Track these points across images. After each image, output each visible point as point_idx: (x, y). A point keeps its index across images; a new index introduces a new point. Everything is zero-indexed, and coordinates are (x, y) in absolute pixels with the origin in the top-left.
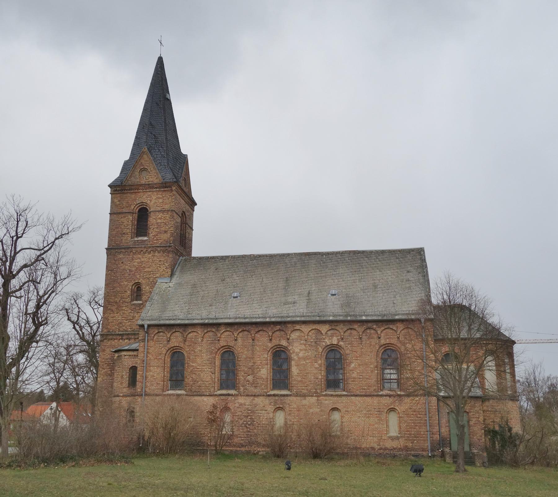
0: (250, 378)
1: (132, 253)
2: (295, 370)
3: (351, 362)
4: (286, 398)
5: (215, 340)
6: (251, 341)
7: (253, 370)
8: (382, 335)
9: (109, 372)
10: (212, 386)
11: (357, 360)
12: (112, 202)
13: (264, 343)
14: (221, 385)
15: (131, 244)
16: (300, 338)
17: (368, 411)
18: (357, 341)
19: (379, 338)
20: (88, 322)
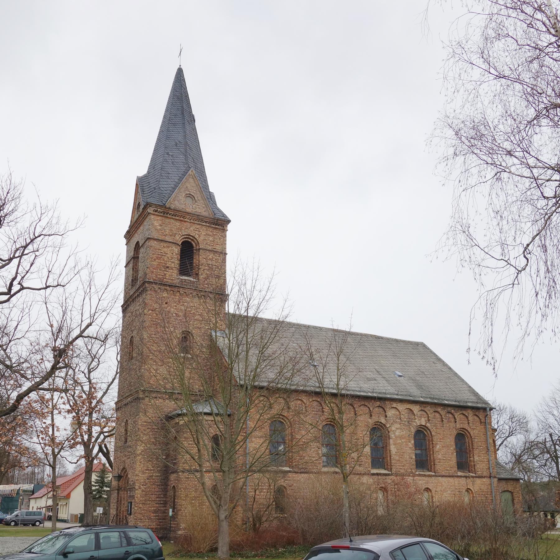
2: (393, 449)
3: (437, 444)
4: (387, 477)
15: (176, 282)
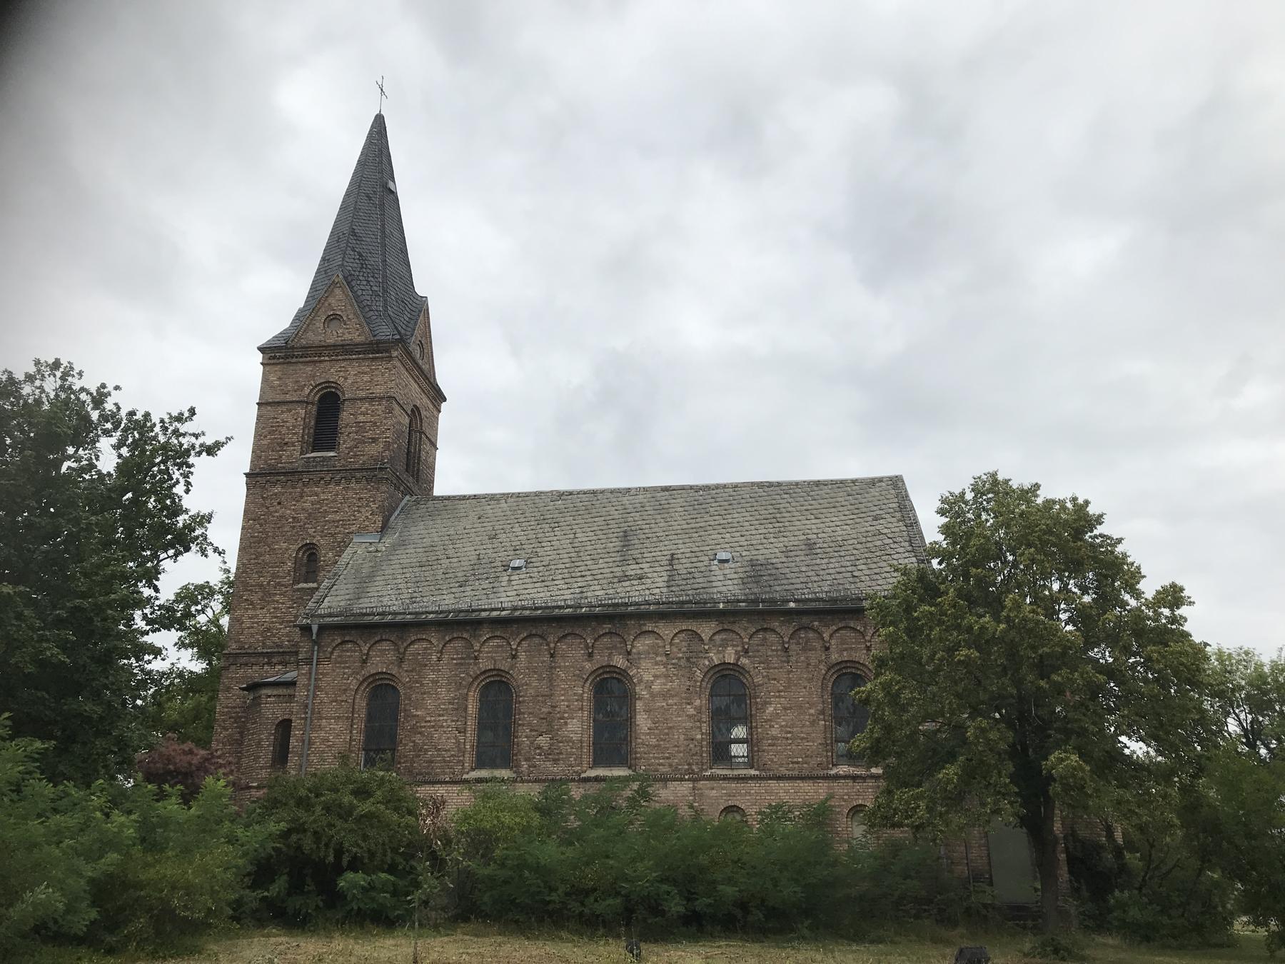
0: (543, 741)
1: (300, 484)
2: (643, 721)
3: (766, 703)
5: (469, 657)
6: (547, 658)
7: (550, 723)
8: (833, 642)
9: (237, 736)
10: (459, 761)
11: (779, 697)
12: (265, 380)
13: (572, 669)
14: (479, 755)
15: (298, 465)
16: (654, 651)
18: (778, 656)
19: (827, 649)
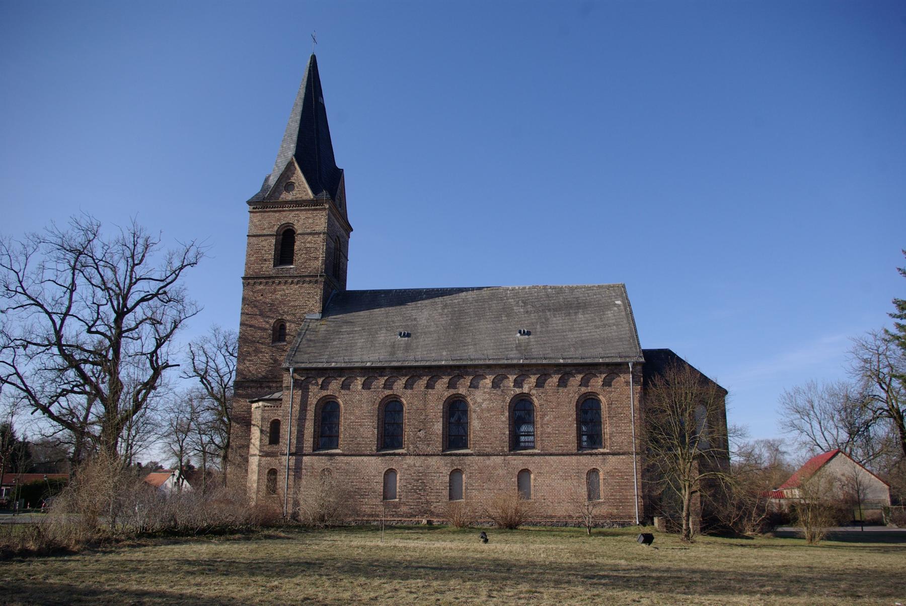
17: (565, 472)
20: (217, 371)
